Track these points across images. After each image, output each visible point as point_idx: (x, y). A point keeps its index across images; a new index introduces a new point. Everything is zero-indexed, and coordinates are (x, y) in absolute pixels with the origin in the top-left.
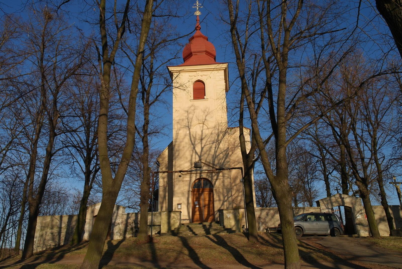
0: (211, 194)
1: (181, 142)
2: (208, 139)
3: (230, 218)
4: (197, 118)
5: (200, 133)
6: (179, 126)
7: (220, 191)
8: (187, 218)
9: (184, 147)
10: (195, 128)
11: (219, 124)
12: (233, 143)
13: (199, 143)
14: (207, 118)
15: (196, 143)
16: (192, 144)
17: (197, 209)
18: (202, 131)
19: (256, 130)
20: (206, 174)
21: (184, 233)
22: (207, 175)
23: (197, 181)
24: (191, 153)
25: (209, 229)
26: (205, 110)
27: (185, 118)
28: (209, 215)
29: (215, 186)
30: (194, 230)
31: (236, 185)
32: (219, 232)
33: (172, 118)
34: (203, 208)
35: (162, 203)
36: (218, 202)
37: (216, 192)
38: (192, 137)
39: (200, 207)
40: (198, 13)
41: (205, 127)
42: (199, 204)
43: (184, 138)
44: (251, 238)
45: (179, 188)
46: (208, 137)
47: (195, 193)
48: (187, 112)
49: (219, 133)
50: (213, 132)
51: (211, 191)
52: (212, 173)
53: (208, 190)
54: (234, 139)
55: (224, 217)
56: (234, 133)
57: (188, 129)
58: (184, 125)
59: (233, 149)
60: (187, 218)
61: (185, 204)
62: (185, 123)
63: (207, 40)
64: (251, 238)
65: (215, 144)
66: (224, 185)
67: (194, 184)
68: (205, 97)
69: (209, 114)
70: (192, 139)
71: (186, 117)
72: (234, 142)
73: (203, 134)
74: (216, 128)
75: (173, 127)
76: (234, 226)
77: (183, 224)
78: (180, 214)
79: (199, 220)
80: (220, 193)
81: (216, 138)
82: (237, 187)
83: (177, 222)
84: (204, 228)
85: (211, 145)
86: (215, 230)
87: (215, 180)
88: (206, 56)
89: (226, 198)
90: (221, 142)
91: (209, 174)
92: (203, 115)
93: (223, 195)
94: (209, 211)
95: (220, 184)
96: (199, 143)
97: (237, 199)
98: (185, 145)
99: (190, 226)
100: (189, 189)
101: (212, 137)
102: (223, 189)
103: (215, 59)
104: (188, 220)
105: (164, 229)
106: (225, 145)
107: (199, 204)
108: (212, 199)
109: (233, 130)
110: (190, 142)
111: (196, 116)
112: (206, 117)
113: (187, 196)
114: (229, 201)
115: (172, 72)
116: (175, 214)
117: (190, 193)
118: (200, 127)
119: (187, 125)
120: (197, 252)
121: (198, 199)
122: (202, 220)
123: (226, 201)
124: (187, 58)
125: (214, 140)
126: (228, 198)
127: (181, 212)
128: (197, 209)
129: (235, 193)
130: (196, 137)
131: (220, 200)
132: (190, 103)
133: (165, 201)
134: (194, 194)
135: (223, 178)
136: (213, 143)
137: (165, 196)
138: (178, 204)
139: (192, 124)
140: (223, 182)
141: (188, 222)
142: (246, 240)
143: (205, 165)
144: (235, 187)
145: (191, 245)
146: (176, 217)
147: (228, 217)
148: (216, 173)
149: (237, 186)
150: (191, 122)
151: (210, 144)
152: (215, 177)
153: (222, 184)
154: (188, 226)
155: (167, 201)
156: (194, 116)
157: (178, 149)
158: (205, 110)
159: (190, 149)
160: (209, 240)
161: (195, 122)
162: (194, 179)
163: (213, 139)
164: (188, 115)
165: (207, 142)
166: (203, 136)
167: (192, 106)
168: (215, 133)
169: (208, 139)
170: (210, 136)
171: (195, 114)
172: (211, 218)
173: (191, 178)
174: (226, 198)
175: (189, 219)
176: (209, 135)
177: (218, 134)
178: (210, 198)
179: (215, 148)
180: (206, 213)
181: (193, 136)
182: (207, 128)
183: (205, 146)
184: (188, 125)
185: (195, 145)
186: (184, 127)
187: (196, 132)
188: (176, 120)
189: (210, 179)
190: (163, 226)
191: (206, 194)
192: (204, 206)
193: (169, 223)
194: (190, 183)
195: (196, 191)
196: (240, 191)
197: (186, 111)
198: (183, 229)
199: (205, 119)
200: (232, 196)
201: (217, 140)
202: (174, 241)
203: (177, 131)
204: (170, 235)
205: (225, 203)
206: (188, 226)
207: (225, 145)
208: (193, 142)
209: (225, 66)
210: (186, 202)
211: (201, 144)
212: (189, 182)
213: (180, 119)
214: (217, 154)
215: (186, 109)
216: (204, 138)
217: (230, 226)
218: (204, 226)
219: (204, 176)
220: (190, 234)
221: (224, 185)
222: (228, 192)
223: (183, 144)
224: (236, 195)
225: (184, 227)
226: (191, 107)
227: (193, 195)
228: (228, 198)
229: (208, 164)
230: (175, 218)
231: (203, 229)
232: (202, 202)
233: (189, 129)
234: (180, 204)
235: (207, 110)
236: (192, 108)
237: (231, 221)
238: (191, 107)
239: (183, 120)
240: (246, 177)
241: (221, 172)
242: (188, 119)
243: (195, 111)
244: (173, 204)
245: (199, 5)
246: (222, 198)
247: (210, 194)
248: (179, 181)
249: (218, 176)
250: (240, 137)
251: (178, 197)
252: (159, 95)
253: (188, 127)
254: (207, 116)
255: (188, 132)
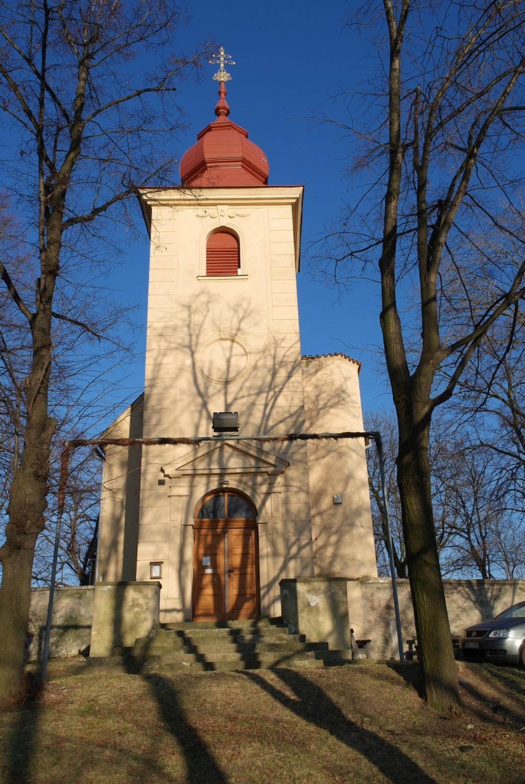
0: (250, 535)
1: (167, 388)
2: (244, 382)
3: (317, 608)
4: (215, 324)
5: (223, 366)
6: (163, 345)
7: (275, 530)
8: (178, 606)
9: (175, 402)
10: (208, 351)
11: (276, 343)
12: (313, 398)
13: (219, 391)
14: (243, 325)
15: (211, 391)
16: (200, 394)
17: (207, 580)
18: (228, 361)
19: (156, 597)
20: (237, 477)
21: (168, 659)
22: (240, 481)
23: (209, 498)
24: (196, 419)
25: (252, 645)
26: (239, 305)
27: (180, 323)
28: (242, 596)
29: (263, 512)
30: (202, 649)
31: (320, 514)
32: (287, 658)
33: (146, 322)
34: (224, 578)
35: (107, 561)
36: (270, 560)
37: (266, 530)
38: (199, 375)
39: (215, 575)
40: (223, 76)
41: (237, 349)
42: (214, 566)
43: (177, 377)
44: (434, 695)
45: (157, 518)
46: (246, 376)
47: (204, 532)
48: (189, 307)
49: (277, 367)
50: (260, 363)
51: (251, 526)
52: (255, 474)
53: (241, 524)
54: (316, 387)
55: (300, 606)
56: (316, 372)
57: (189, 353)
58: (180, 341)
59: (314, 413)
60: (178, 606)
61: (171, 564)
62: (182, 335)
63: (247, 136)
64: (434, 695)
65: (264, 395)
66: (288, 511)
67: (200, 507)
68: (240, 271)
69: (249, 315)
70: (200, 381)
71: (184, 320)
72: (317, 396)
73: (231, 369)
74: (267, 353)
75: (148, 348)
76: (330, 634)
77: (164, 626)
78: (157, 594)
79: (212, 611)
80: (277, 532)
81: (269, 379)
82: (322, 519)
83: (146, 619)
84: (235, 641)
85: (253, 397)
86: (273, 647)
87: (262, 496)
88: (243, 171)
89: (294, 550)
90: (280, 391)
91: (245, 479)
92: (233, 316)
93: (286, 540)
94: (242, 586)
95: (277, 510)
96: (219, 391)
97: (322, 554)
98: (178, 397)
99: (188, 632)
100: (186, 519)
101: (256, 376)
102: (285, 522)
103: (266, 180)
104: (178, 611)
105: (100, 643)
106: (292, 400)
107: (214, 566)
108: (252, 551)
109: (315, 362)
110: (194, 390)
111: (213, 321)
112: (240, 323)
113: (178, 540)
114: (302, 558)
115: (149, 203)
116: (140, 592)
117: (190, 530)
118: (223, 349)
119: (186, 342)
120: (223, 763)
121: (212, 551)
122: (222, 618)
123: (294, 557)
124: (192, 176)
125: (262, 386)
126: (300, 549)
127: (160, 586)
128: (207, 580)
129: (320, 535)
130: (210, 375)
131: (275, 554)
132: (198, 286)
133: (113, 558)
134: (200, 535)
135: (287, 491)
136: (258, 394)
137: (114, 544)
138: (153, 564)
139: (201, 341)
140: (286, 502)
141: (179, 617)
142: (412, 696)
143: (236, 452)
144: (318, 520)
145: (195, 720)
146: (142, 601)
147: (312, 604)
148: (266, 476)
149: (325, 516)
150: (198, 336)
151: (249, 395)
152: (264, 489)
153: (282, 509)
154: (180, 634)
155: (121, 556)
156: (208, 319)
157: (158, 407)
158: (239, 305)
159: (192, 408)
160: (265, 696)
161: (208, 334)
162: (200, 491)
163: (259, 383)
164: (190, 316)
165: (241, 389)
166: (232, 374)
167: (203, 292)
168: (265, 366)
169: (244, 382)
170: (250, 374)
171: (210, 314)
172: (248, 606)
173: (192, 487)
174: (294, 550)
175: (183, 610)
176: (249, 371)
177: (274, 368)
178: (245, 546)
179: (266, 405)
180: (232, 592)
181: (202, 371)
182: (242, 351)
183: (235, 399)
184: (191, 341)
185: (208, 397)
186: (177, 348)
187: (211, 362)
188: (155, 329)
189: (248, 493)
190: (99, 632)
191: (234, 539)
192: (229, 571)
193: (117, 621)
194: (189, 503)
195: (206, 525)
196: (334, 530)
197: (184, 306)
198: (165, 643)
199: (239, 329)
200: (310, 542)
201: (271, 387)
202: (126, 698)
203: (156, 359)
204: (119, 664)
205: (292, 564)
206: (180, 634)
207: (292, 400)
208: (202, 389)
209: (296, 192)
210: (175, 558)
211: (226, 394)
212: (185, 499)
213: (166, 327)
214: (271, 423)
215: (186, 301)
216: (234, 379)
217: (319, 633)
218: (236, 635)
219: (232, 482)
220: (187, 661)
221: (288, 511)
222: (299, 532)
223: (173, 393)
224: (320, 542)
225: (168, 635)
226: (198, 296)
227: (198, 538)
228: (300, 549)
229: (245, 449)
230: (138, 605)
231: (233, 646)
232: (221, 560)
233: (193, 354)
234: (159, 564)
235: (245, 305)
236: (203, 298)
237: (321, 619)
238: (198, 296)
239: (175, 329)
240: (407, 459)
241: (283, 472)
242: (189, 326)
243: (210, 306)
244: (139, 564)
245: (225, 59)
246: (281, 548)
247: (246, 537)
248: (158, 497)
249: (271, 485)
250: (383, 316)
251: (153, 542)
252: (104, 208)
253: (190, 347)
254: (245, 320)
255: (189, 362)
